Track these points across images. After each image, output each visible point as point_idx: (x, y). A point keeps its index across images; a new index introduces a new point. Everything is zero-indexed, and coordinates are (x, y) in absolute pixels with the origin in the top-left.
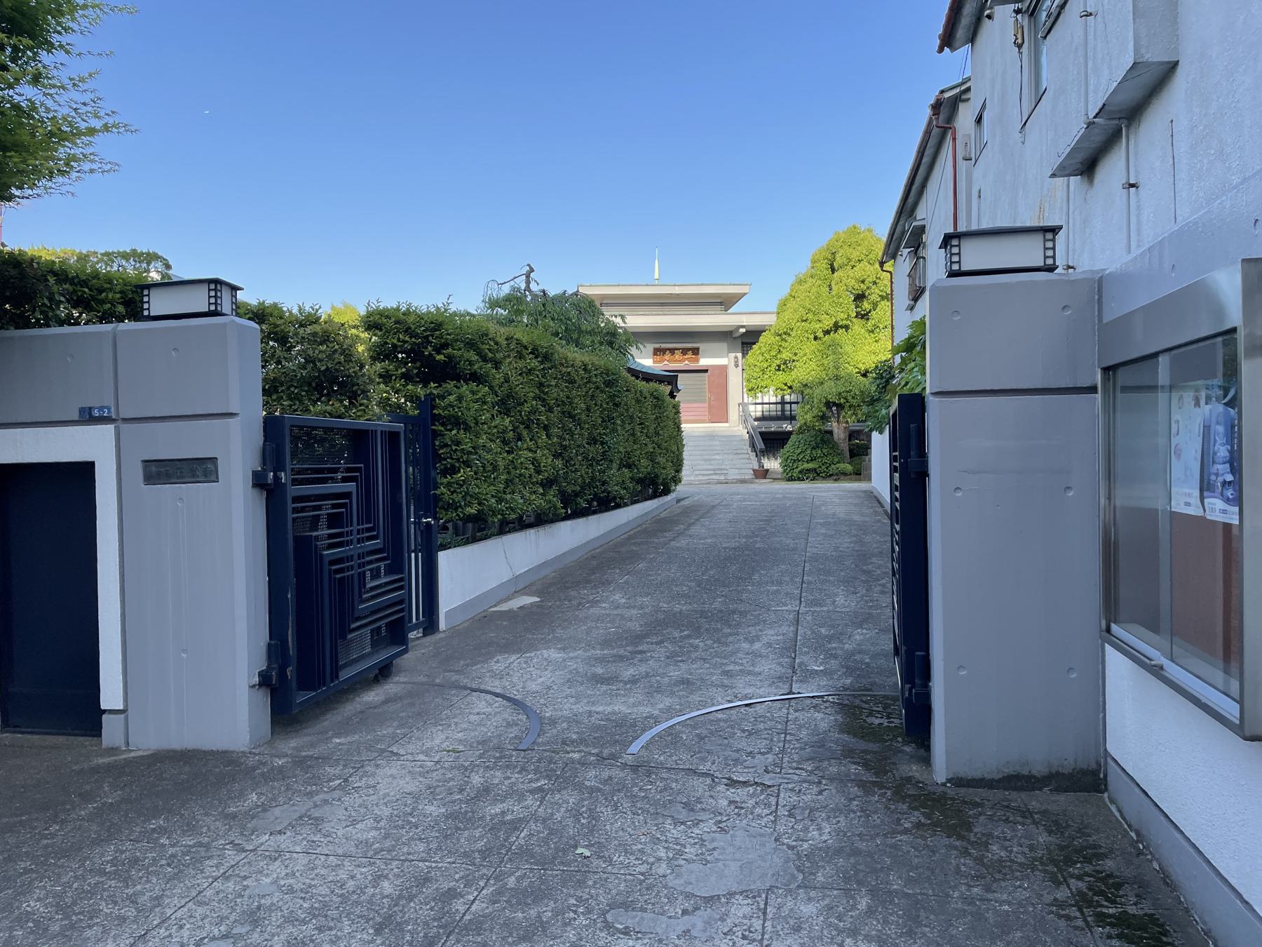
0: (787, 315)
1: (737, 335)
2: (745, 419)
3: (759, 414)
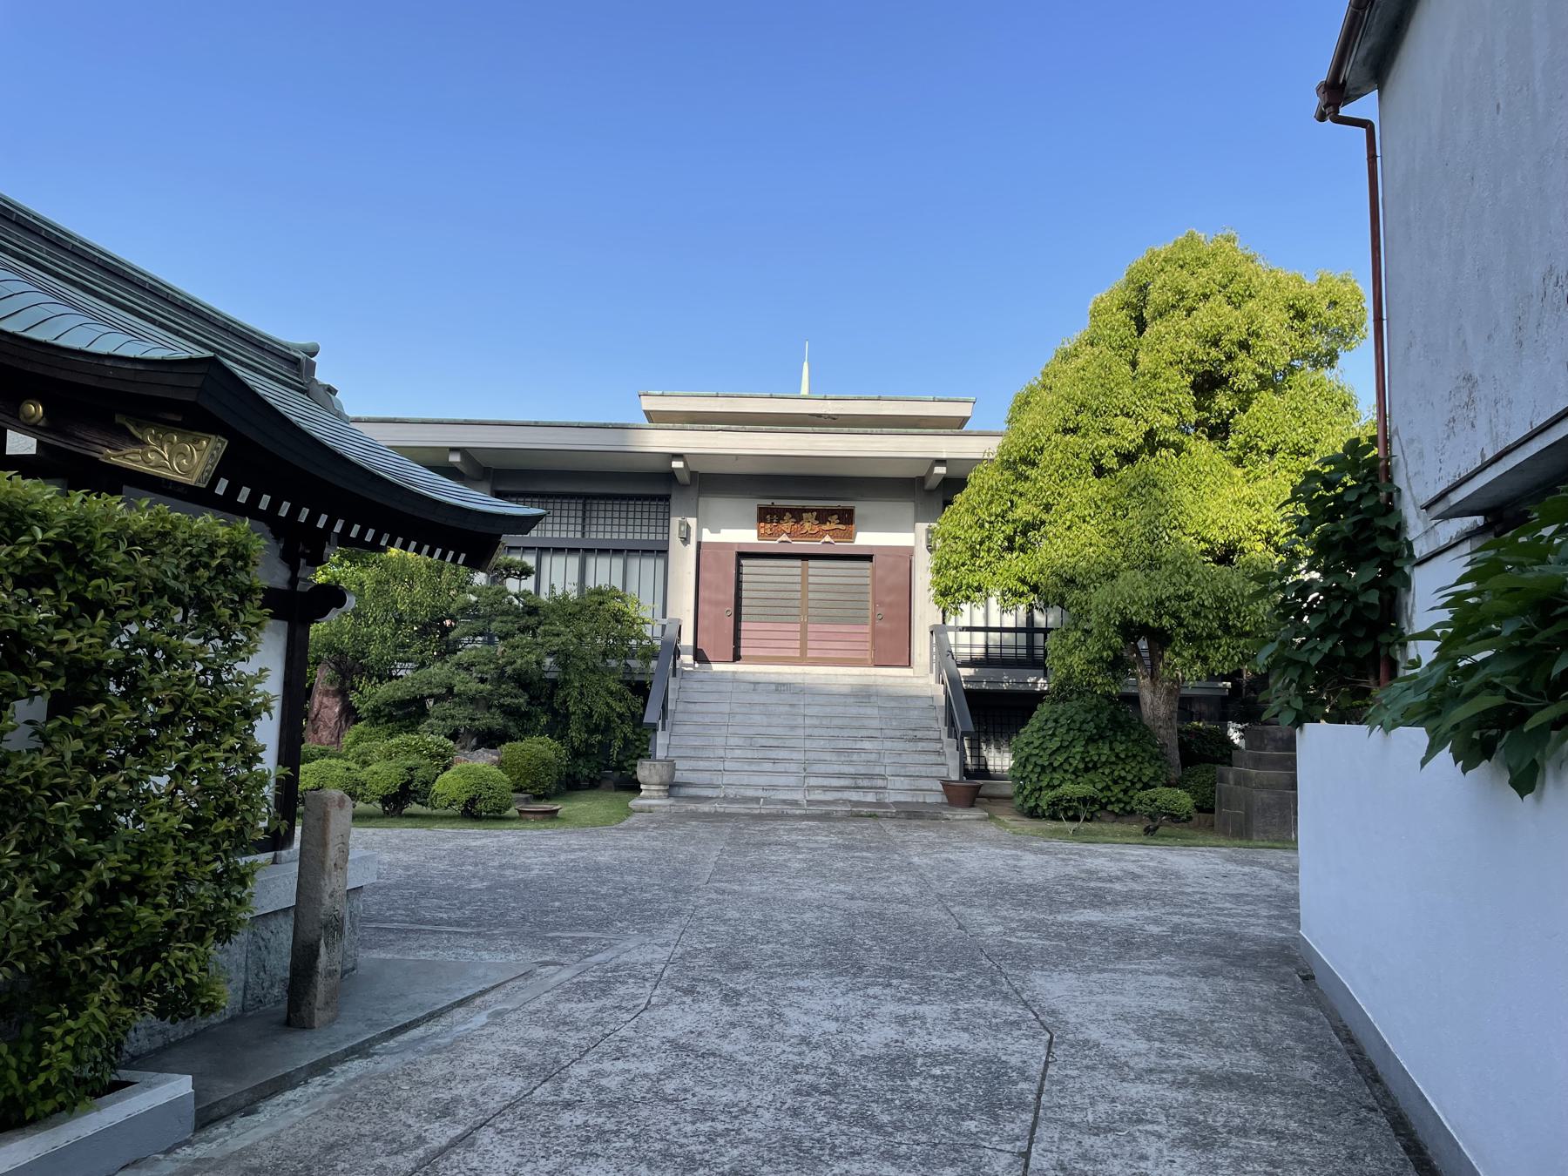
0: (1029, 420)
1: (932, 483)
2: (943, 652)
3: (979, 652)
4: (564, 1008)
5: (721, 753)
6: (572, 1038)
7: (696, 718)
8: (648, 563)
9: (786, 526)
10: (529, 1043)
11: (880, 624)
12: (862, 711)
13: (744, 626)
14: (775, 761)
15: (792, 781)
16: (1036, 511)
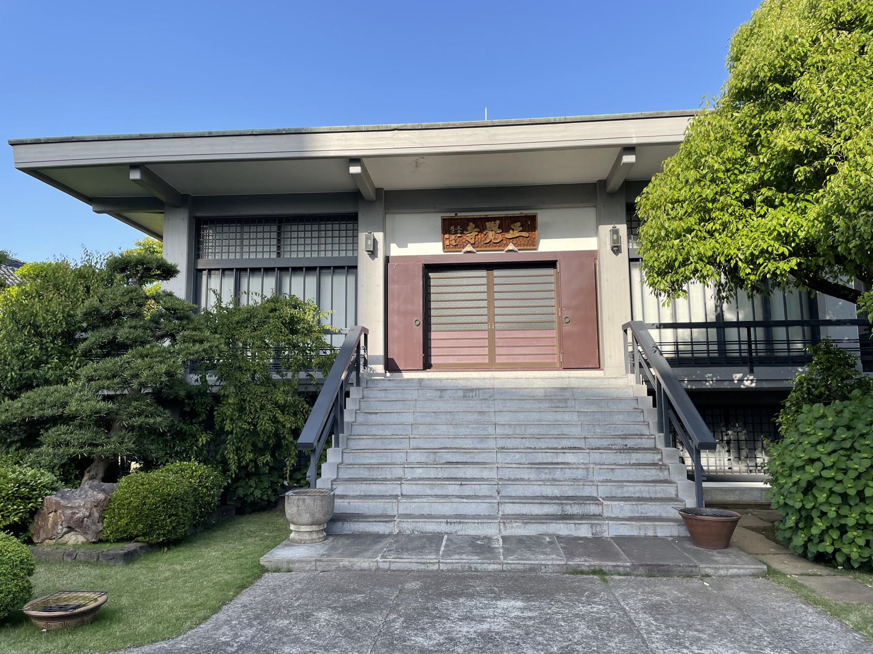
5: (399, 472)
7: (374, 430)
8: (340, 280)
9: (470, 236)
11: (567, 328)
12: (559, 416)
13: (433, 335)
14: (462, 481)
15: (482, 508)
16: (810, 134)
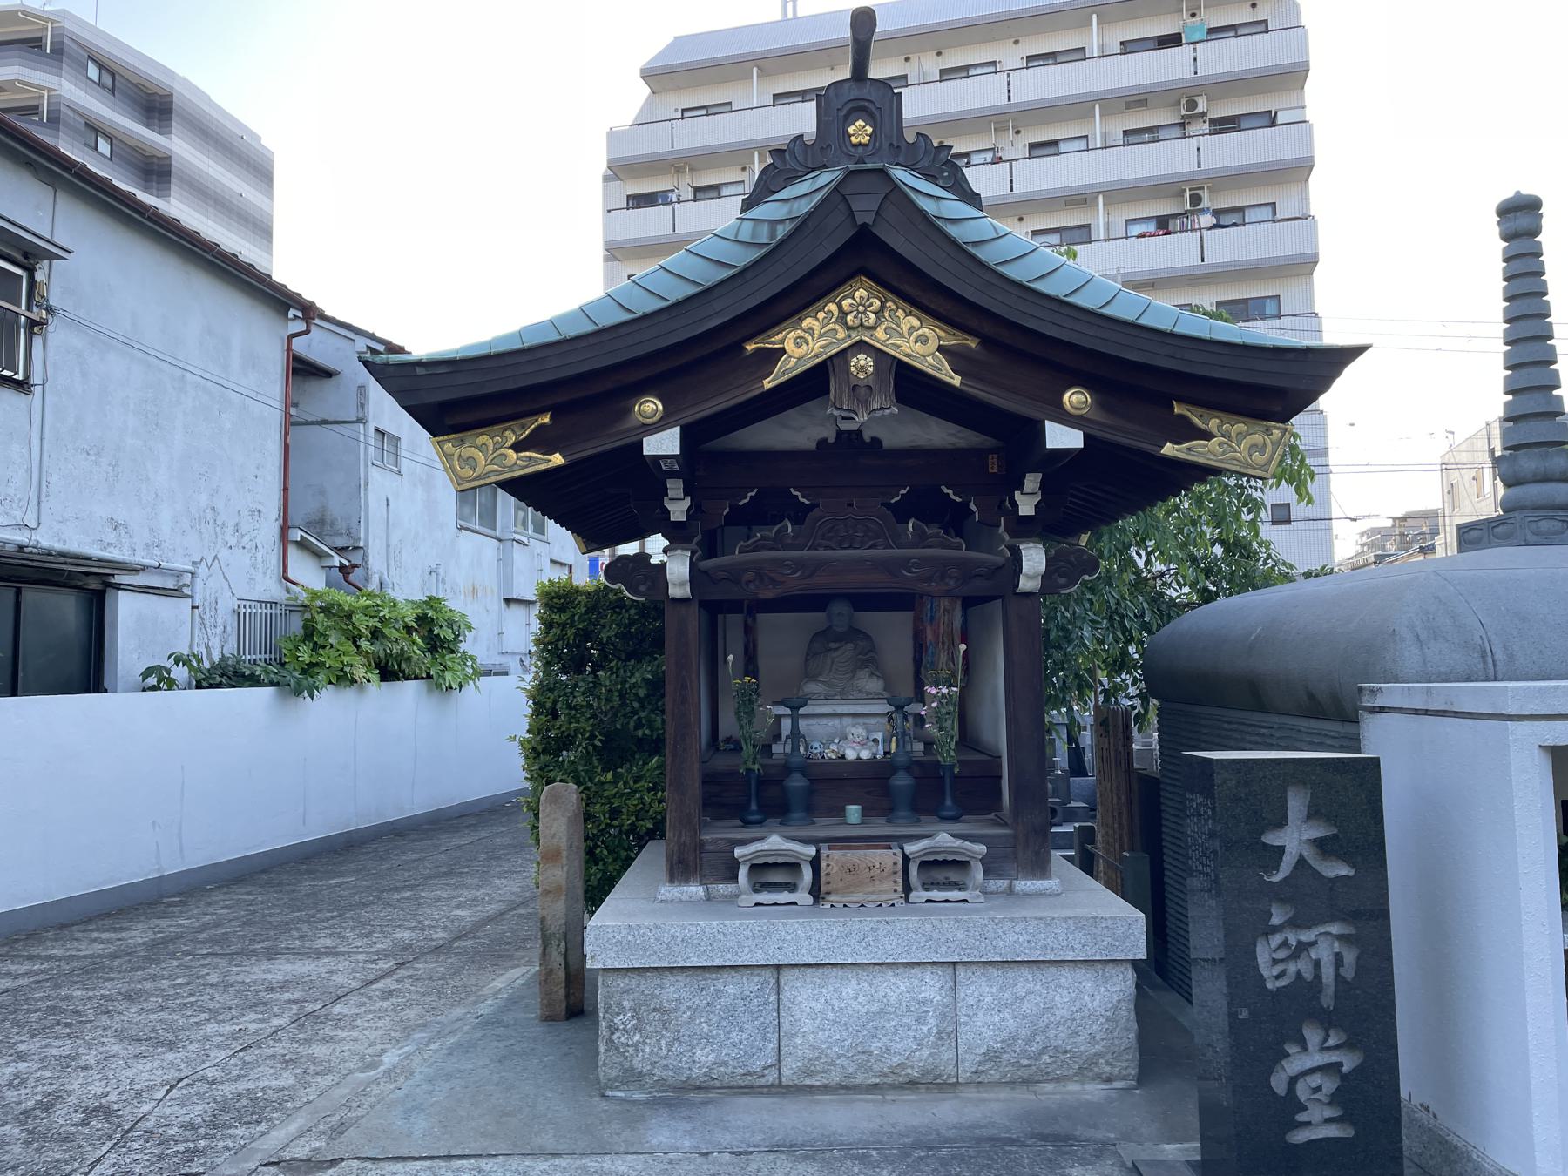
4: (287, 1079)
6: (280, 1048)
10: (326, 1040)
